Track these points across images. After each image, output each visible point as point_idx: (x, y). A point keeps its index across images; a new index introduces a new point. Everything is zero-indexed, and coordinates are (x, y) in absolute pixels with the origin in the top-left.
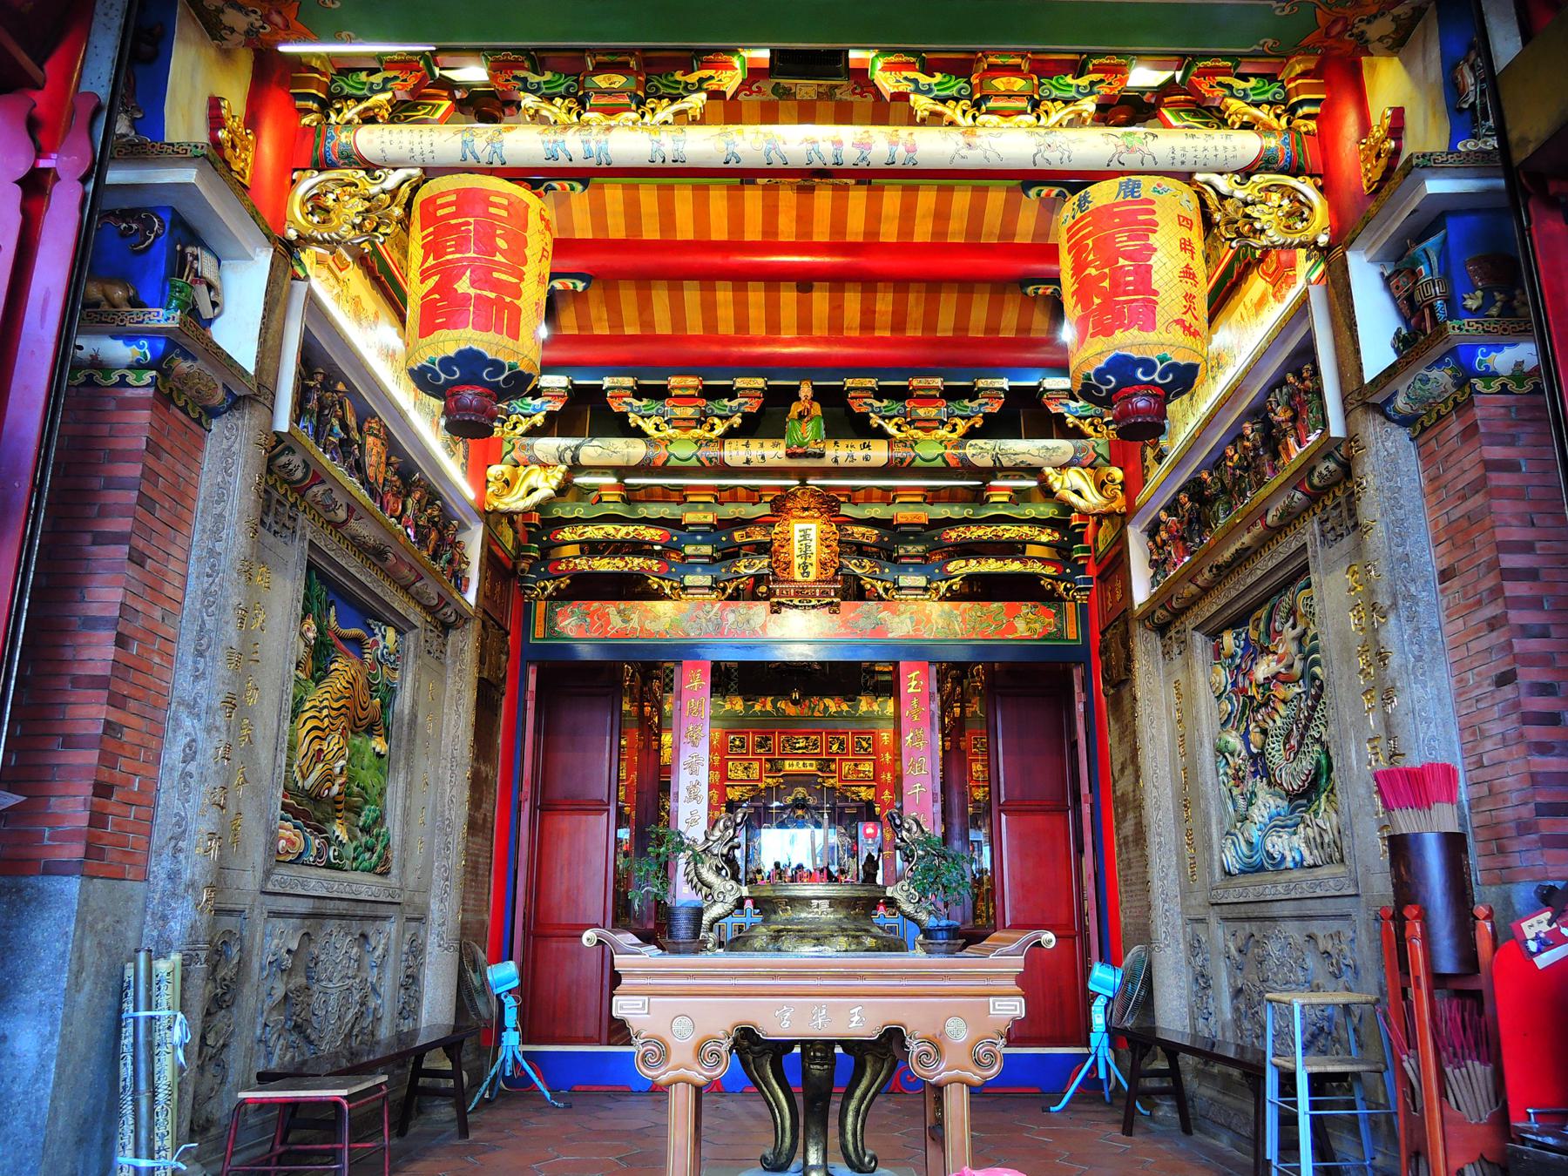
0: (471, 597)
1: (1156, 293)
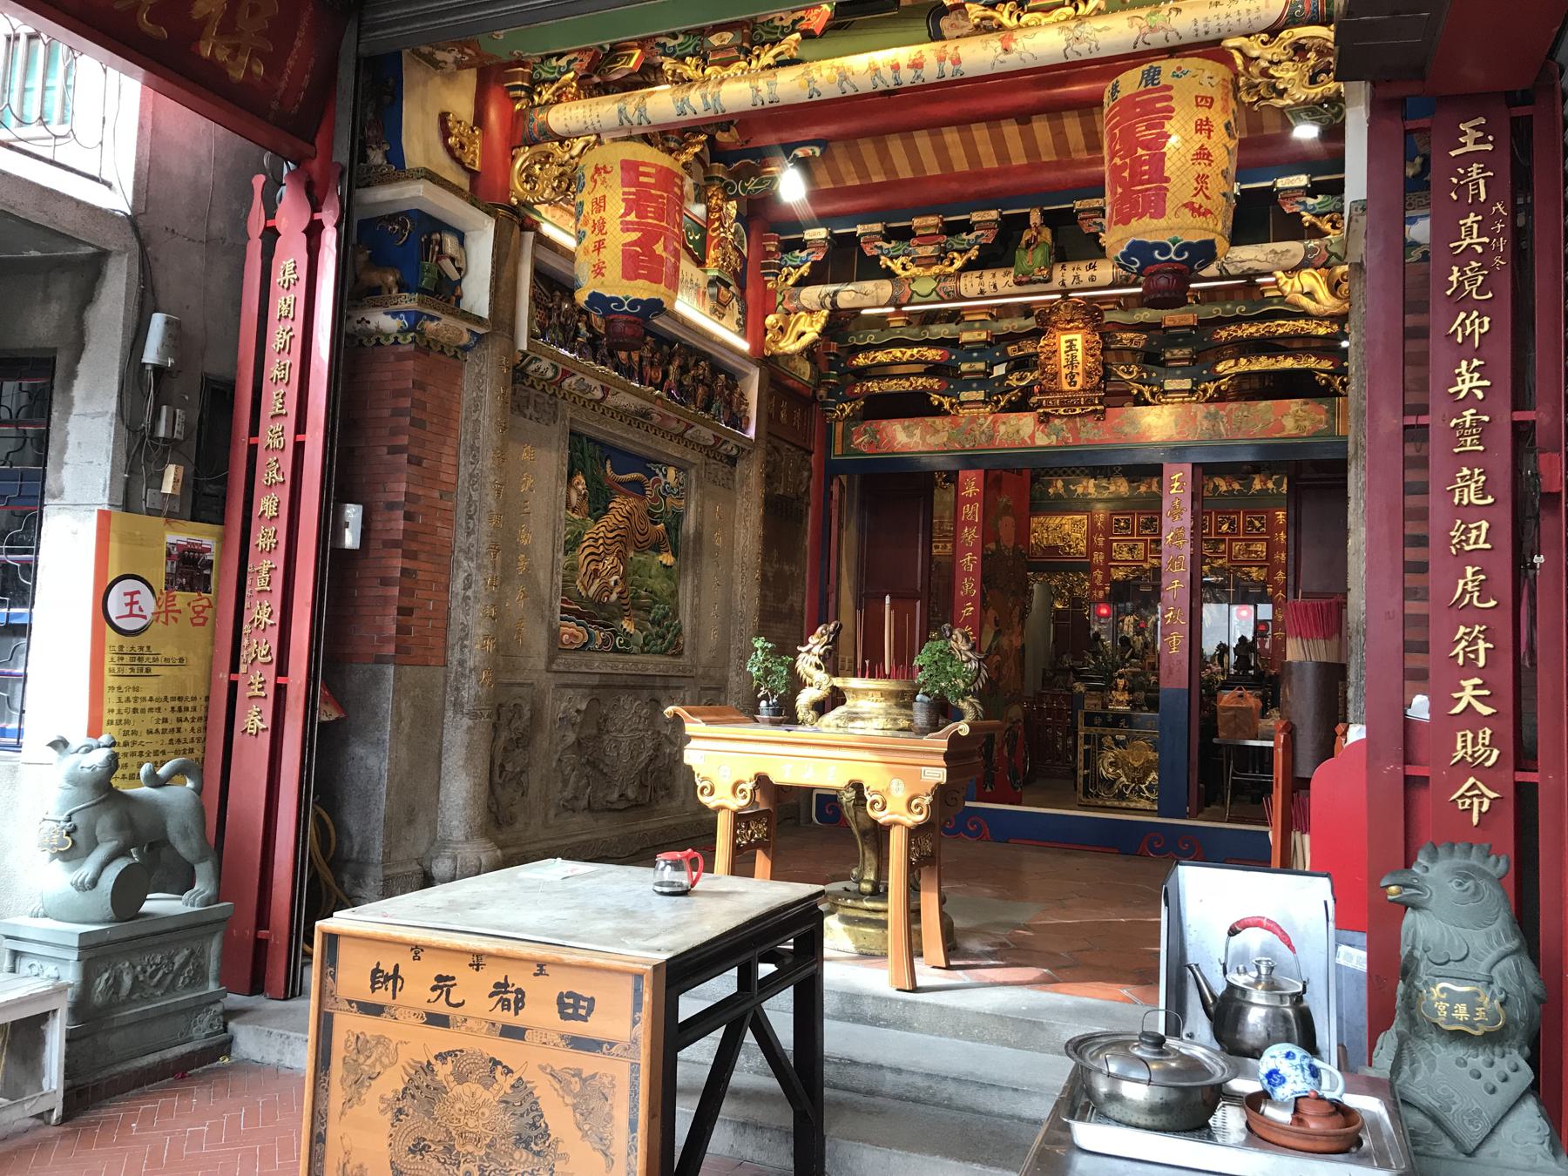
0: (751, 433)
1: (1167, 180)
